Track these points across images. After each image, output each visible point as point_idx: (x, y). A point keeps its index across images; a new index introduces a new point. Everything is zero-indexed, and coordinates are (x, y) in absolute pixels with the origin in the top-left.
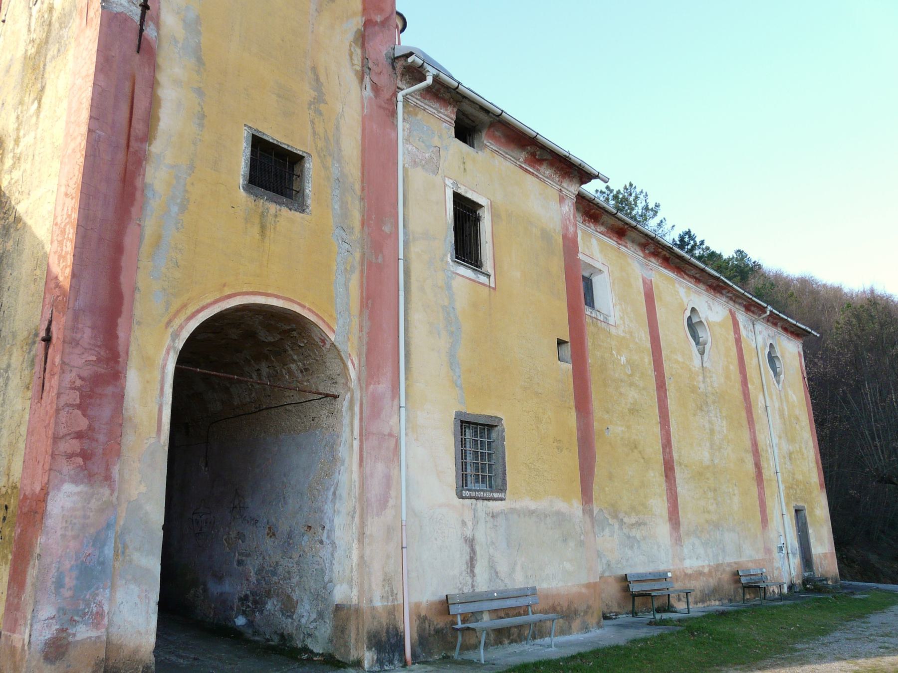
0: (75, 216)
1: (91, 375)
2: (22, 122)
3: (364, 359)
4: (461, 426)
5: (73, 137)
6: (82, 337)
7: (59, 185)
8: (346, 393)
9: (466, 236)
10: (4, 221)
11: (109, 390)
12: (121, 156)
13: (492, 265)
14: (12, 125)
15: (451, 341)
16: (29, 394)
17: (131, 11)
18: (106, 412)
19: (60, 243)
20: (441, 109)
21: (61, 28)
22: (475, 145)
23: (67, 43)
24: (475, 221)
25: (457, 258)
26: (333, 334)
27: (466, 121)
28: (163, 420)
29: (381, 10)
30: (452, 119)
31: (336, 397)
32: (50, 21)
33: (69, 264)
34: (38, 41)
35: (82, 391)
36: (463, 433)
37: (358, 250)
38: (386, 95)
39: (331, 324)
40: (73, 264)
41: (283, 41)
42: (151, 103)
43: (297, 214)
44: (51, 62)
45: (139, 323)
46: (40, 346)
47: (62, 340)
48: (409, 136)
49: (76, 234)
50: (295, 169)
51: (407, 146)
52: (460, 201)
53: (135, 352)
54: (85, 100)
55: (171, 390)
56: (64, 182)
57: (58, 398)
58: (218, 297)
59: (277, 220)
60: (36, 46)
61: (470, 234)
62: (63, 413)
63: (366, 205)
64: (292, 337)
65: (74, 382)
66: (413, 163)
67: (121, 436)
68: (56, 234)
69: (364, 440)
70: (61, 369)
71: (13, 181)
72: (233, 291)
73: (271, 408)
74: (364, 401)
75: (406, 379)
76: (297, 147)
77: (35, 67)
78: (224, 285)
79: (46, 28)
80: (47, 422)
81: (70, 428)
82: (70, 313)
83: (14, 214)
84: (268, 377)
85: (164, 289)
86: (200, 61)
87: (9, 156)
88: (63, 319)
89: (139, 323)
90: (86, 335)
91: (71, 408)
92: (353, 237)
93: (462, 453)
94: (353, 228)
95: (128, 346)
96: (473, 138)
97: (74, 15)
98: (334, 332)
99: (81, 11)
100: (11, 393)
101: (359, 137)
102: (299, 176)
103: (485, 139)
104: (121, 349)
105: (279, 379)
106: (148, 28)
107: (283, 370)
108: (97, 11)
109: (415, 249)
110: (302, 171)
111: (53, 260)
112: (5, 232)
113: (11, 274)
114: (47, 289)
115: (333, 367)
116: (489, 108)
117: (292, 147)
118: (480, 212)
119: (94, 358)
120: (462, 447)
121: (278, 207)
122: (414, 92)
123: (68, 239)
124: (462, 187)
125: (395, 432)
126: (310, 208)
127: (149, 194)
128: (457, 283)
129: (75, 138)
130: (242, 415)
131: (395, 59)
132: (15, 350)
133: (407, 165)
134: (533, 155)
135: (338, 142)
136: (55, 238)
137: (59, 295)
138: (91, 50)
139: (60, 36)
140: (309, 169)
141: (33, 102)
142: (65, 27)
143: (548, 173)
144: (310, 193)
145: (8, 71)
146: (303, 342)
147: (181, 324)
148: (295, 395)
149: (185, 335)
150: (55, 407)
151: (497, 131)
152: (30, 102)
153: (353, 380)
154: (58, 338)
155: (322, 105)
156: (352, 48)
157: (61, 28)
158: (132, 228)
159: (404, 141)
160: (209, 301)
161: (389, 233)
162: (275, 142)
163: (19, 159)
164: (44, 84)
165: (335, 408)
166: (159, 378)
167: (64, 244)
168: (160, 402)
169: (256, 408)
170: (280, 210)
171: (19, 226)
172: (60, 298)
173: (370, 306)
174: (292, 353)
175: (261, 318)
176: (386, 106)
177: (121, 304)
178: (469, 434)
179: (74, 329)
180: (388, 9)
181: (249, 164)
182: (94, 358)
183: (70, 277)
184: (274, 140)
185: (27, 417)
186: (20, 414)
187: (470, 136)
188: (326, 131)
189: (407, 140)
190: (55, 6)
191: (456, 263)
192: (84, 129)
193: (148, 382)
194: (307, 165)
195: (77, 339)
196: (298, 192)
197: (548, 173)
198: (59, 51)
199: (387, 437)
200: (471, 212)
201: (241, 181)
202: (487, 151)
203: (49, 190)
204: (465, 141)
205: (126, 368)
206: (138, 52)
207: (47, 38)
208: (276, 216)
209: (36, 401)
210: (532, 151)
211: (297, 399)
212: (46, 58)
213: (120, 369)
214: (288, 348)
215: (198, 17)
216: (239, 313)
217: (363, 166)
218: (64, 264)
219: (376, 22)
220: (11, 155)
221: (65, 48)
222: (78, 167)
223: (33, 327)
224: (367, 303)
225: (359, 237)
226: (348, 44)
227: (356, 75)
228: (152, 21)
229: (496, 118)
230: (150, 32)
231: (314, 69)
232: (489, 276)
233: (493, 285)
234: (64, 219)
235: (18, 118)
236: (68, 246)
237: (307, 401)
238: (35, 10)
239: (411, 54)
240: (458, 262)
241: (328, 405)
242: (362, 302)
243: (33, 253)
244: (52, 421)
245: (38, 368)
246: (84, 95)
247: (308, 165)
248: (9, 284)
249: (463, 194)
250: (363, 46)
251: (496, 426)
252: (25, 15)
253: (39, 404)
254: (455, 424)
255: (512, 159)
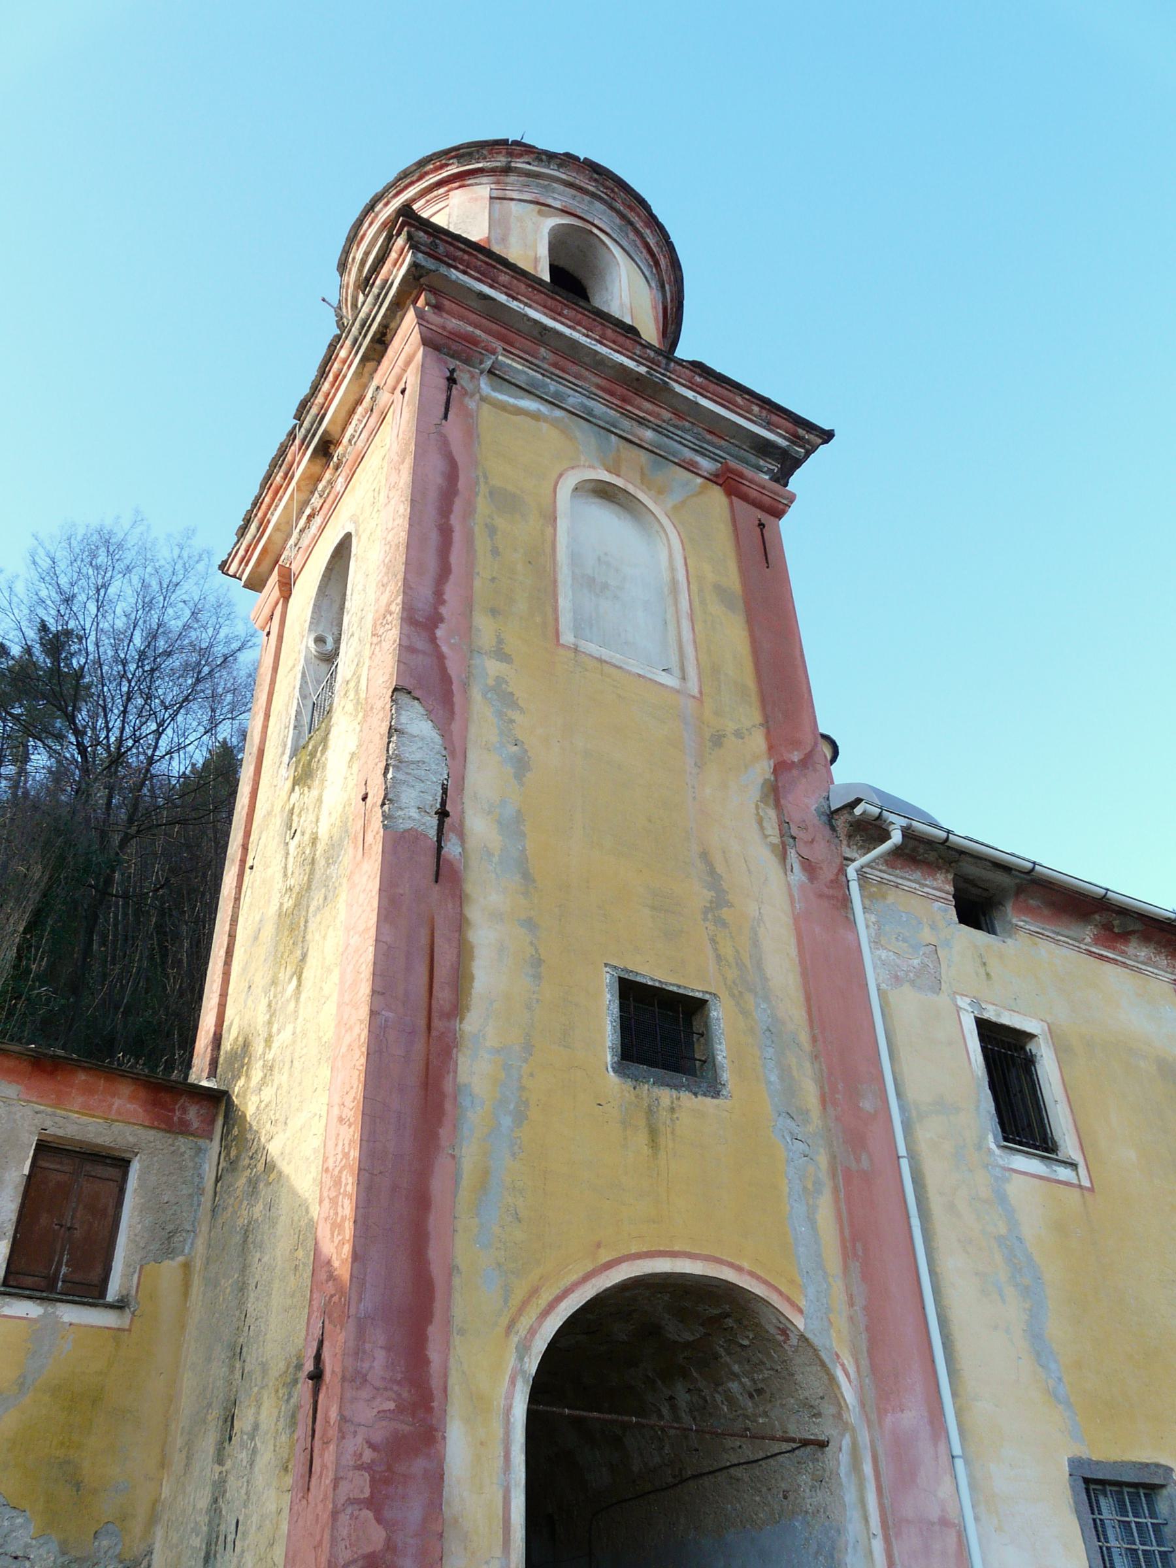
0: (355, 1154)
1: (387, 1439)
2: (275, 1010)
3: (865, 1362)
4: (1087, 1491)
5: (348, 1026)
6: (371, 1367)
7: (330, 1105)
8: (843, 1435)
9: (1015, 1095)
10: (249, 1170)
11: (419, 1465)
12: (419, 1046)
13: (1078, 1145)
14: (262, 1017)
15: (1027, 1306)
16: (289, 1480)
17: (424, 824)
18: (414, 1512)
19: (334, 1201)
20: (926, 880)
21: (328, 865)
22: (998, 929)
23: (337, 884)
24: (1026, 1065)
25: (1006, 1139)
26: (799, 1316)
27: (974, 890)
28: (513, 1516)
29: (796, 744)
30: (948, 893)
31: (822, 1445)
32: (313, 858)
33: (347, 1238)
34: (297, 888)
35: (374, 1471)
36: (1094, 1507)
37: (822, 1151)
38: (828, 874)
39: (794, 1298)
40: (354, 1236)
41: (650, 821)
42: (459, 956)
43: (708, 1100)
44: (314, 916)
45: (462, 1332)
46: (304, 1388)
47: (340, 1376)
48: (878, 935)
49: (358, 1184)
50: (694, 1023)
51: (878, 952)
52: (988, 1031)
53: (457, 1388)
54: (364, 966)
55: (523, 1457)
56: (336, 1099)
57: (335, 1487)
58: (590, 1267)
59: (675, 1116)
60: (294, 896)
61: (1021, 1091)
62: (344, 1518)
63: (824, 1068)
64: (725, 1329)
65: (361, 1455)
66: (893, 980)
67: (441, 1559)
68: (327, 1188)
69: (893, 1539)
70: (340, 1430)
71: (263, 1105)
72: (614, 1255)
73: (702, 1475)
74: (880, 1451)
75: (954, 1394)
76: (694, 987)
77: (294, 926)
78: (599, 1245)
79: (308, 868)
80: (318, 1537)
81: (355, 1549)
82: (351, 1325)
83: (264, 1158)
84: (691, 1411)
85: (499, 1265)
86: (527, 876)
87: (258, 1066)
88: (341, 1338)
89: (462, 1332)
90: (378, 1364)
91: (356, 1507)
92: (811, 1128)
93: (1103, 1556)
94: (808, 1111)
95: (446, 1376)
96: (990, 919)
97: (345, 843)
98: (801, 1311)
99: (356, 838)
100: (259, 1480)
101: (793, 952)
102: (702, 1035)
103: (1012, 914)
104: (435, 1383)
105: (711, 1415)
106: (449, 844)
107: (717, 1396)
108: (377, 833)
109: (925, 1134)
110: (706, 1025)
111: (324, 1231)
112: (250, 1189)
113: (260, 1260)
114: (315, 1285)
115: (810, 1383)
116: (1010, 863)
117: (685, 987)
118: (1031, 1046)
119: (391, 1405)
120: (1093, 1513)
121: (674, 1093)
122: (873, 861)
123: (345, 1194)
124: (991, 1008)
125: (952, 1515)
126: (729, 1086)
127: (465, 1101)
128: (1016, 1189)
129: (351, 1028)
130: (649, 1493)
131: (832, 815)
132: (265, 1397)
133: (883, 986)
134: (1107, 927)
135: (759, 966)
136: (325, 1194)
137: (333, 1292)
138: (371, 891)
139: (327, 877)
140: (718, 1019)
141: (291, 979)
142: (334, 863)
143: (1143, 954)
144: (725, 1061)
145: (256, 938)
146: (748, 1337)
147: (531, 1327)
148: (744, 1446)
149: (540, 1345)
150: (331, 1506)
151: (1032, 899)
152: (287, 980)
153: (850, 1406)
154: (333, 1372)
155: (725, 909)
156: (760, 811)
157: (328, 865)
158: (442, 1164)
159: (872, 944)
160: (574, 1277)
161: (872, 1111)
162: (657, 984)
163: (271, 1068)
164: (305, 950)
165: (824, 1470)
166: (500, 1433)
167: (340, 1204)
168: (505, 1484)
169: (674, 1477)
170: (678, 1099)
171: (272, 1176)
172: (336, 1299)
173: (860, 1253)
174: (728, 1360)
175: (666, 1298)
176: (831, 892)
177: (431, 1299)
178: (1108, 1510)
179: (358, 1353)
180: (809, 740)
181: (618, 1027)
182: (391, 1405)
183: (350, 1260)
184: (655, 980)
185: (285, 1527)
186: (274, 1522)
187: (984, 915)
188: (737, 951)
189: (876, 943)
190: (319, 837)
191: (1007, 1151)
192: (364, 1012)
193: (482, 1444)
194: (714, 1014)
195: (364, 1371)
196: (705, 1062)
197: (1143, 954)
198: (325, 898)
199: (937, 1528)
200: (1016, 1050)
201: (609, 1058)
202: (1022, 936)
203: (316, 1115)
204: (978, 926)
205: (445, 1418)
206: (437, 882)
207: (310, 881)
208: (672, 1110)
209: (300, 1495)
210: (1104, 921)
211: (749, 1453)
212: (307, 911)
213: (434, 1421)
214: (722, 1352)
215: (519, 811)
216: (627, 1294)
217: (808, 999)
218: (340, 1238)
219: (793, 762)
220: (261, 1063)
221: (334, 892)
222: (357, 1072)
223: (294, 1353)
224: (854, 1246)
225: (820, 1127)
226: (754, 806)
227: (773, 851)
228: (453, 832)
229: (1025, 876)
230: (452, 848)
231: (705, 856)
232: (1073, 1165)
233: (1086, 1183)
234: (339, 1160)
235: (269, 1005)
236: (345, 1206)
237: (767, 1457)
238: (293, 844)
239: (858, 801)
240: (1010, 1148)
241: (810, 1464)
242: (844, 1247)
243: (292, 1221)
244: (327, 1536)
245: (302, 1431)
246: (362, 960)
247: (715, 1014)
248: (257, 1277)
249: (994, 1019)
250: (778, 805)
251: (1163, 1486)
252: (280, 856)
253: (304, 1502)
254: (1073, 1488)
255: (1071, 942)
